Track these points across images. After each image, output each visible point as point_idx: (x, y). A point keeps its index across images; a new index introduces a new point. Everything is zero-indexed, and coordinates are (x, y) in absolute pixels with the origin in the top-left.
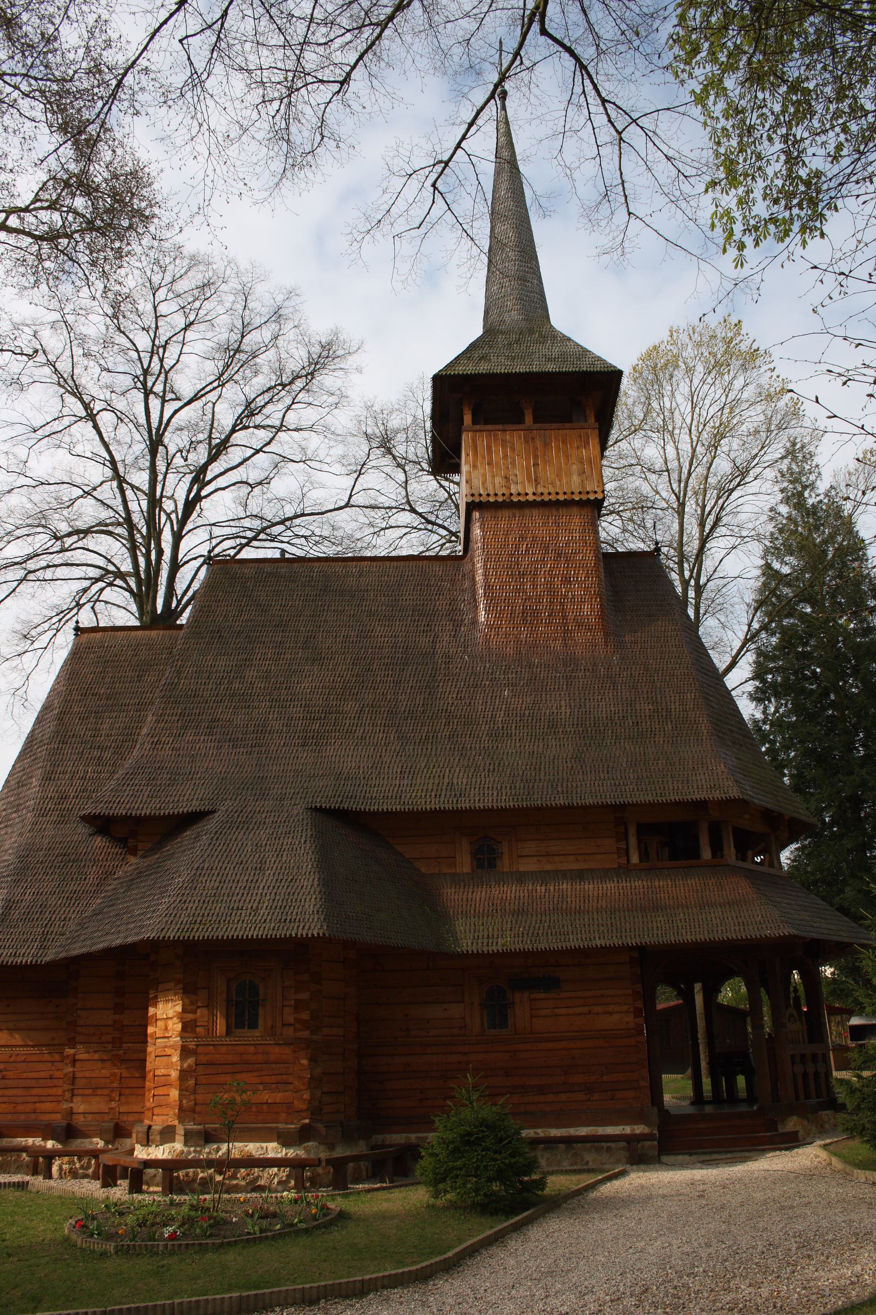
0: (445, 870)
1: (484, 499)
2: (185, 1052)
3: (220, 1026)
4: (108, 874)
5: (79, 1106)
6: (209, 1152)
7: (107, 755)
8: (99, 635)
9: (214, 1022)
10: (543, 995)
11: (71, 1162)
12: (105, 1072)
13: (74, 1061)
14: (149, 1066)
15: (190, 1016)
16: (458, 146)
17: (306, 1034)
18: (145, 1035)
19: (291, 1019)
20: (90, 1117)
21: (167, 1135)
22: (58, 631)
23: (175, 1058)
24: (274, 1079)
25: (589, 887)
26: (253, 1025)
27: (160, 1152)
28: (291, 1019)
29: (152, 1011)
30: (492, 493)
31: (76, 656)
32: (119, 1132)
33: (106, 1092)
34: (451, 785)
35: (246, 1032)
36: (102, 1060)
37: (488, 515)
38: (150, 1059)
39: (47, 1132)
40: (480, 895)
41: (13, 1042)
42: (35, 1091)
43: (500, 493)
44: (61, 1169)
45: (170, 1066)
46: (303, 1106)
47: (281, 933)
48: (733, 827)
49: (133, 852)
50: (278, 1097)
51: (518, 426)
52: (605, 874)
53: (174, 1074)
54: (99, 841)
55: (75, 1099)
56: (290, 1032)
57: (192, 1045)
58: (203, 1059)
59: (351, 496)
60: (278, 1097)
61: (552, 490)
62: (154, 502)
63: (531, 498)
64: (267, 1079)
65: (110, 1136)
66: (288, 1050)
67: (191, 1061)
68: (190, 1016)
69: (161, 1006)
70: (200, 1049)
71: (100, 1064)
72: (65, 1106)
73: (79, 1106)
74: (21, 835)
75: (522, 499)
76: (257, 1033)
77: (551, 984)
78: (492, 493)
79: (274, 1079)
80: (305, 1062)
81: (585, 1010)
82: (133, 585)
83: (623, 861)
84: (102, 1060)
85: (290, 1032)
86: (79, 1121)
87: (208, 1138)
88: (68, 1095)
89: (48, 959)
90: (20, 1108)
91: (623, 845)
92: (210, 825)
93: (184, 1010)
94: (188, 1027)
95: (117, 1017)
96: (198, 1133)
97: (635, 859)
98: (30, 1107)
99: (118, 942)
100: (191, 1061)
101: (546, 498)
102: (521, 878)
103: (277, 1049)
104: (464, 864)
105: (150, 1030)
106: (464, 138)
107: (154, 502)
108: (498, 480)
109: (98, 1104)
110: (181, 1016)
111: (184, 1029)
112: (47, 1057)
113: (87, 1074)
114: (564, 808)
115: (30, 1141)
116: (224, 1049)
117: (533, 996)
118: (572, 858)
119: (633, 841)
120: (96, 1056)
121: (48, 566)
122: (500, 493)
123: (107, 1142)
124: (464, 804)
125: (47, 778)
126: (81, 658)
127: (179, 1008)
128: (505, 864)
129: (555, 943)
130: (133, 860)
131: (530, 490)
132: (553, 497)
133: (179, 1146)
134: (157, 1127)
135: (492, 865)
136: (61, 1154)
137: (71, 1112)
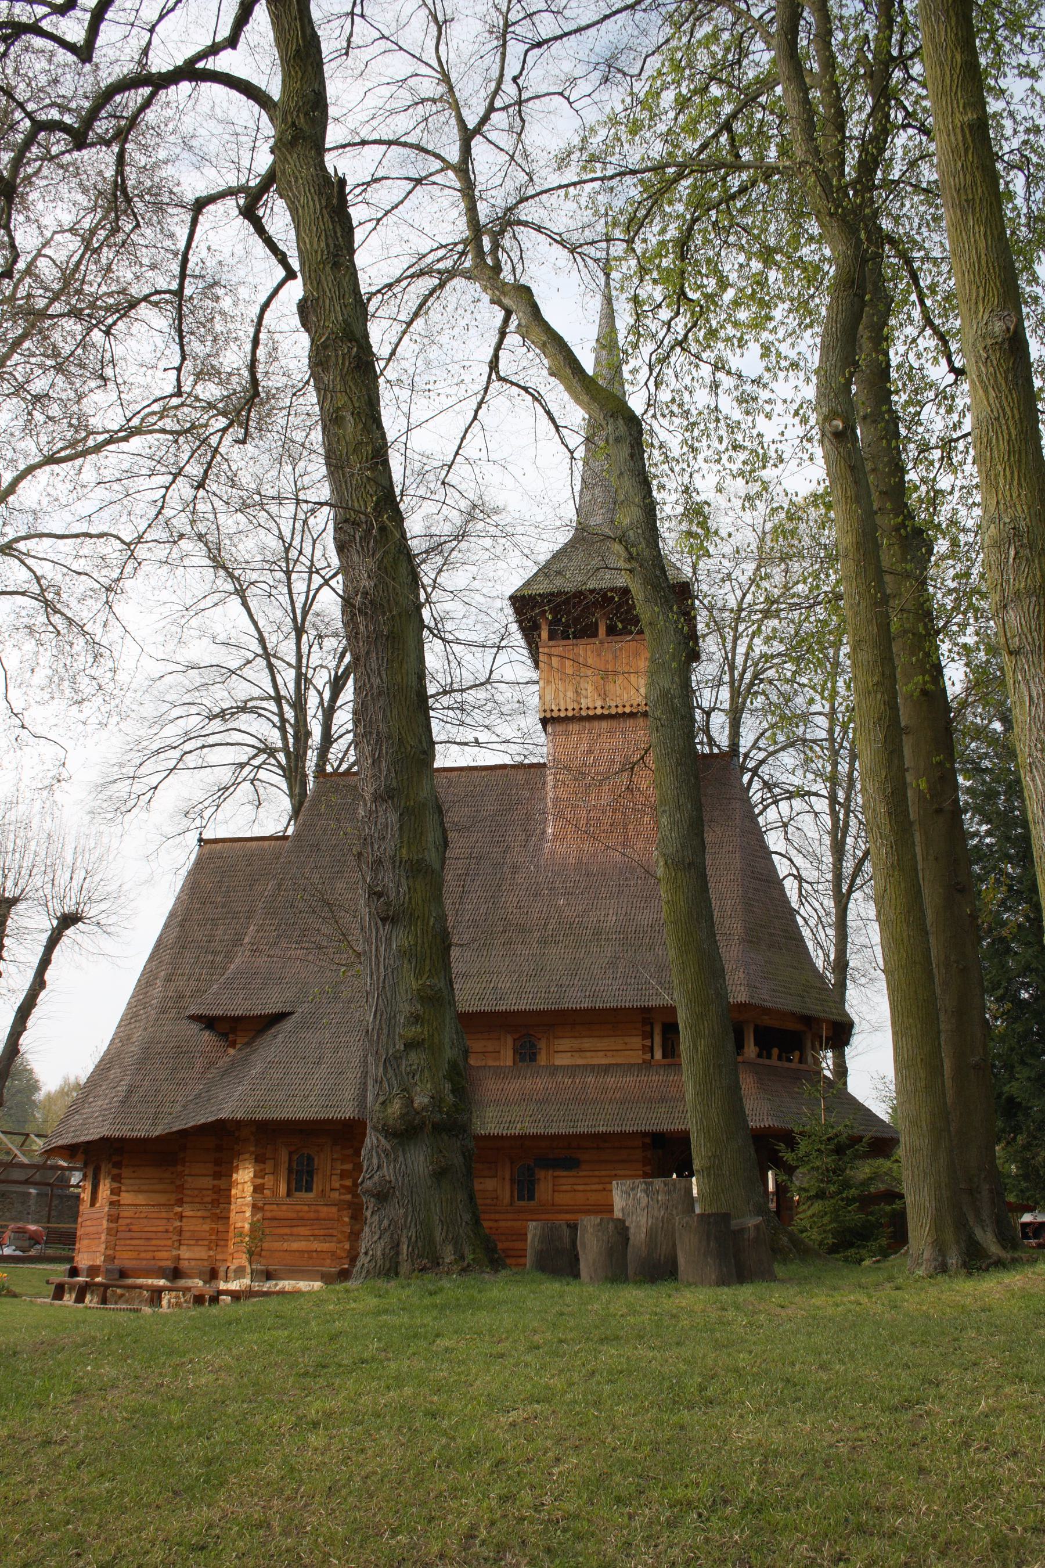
0: (491, 1063)
1: (555, 714)
2: (255, 1207)
3: (283, 1189)
4: (212, 1064)
5: (185, 1253)
6: (268, 1286)
7: (219, 959)
8: (219, 846)
9: (278, 1186)
10: (565, 1173)
11: (177, 1297)
12: (206, 1227)
13: (181, 1217)
14: (232, 1221)
15: (259, 1181)
16: (457, 453)
17: (349, 1197)
18: (229, 1196)
19: (337, 1185)
20: (193, 1263)
21: (240, 1273)
22: (218, 806)
23: (248, 1214)
24: (322, 1232)
25: (611, 1080)
26: (309, 1189)
27: (234, 1286)
28: (337, 1185)
29: (235, 1176)
30: (563, 708)
31: (200, 866)
32: (213, 1275)
33: (206, 1243)
34: (495, 988)
35: (303, 1195)
36: (203, 1218)
37: (559, 728)
38: (232, 1215)
39: (161, 1273)
40: (514, 1086)
41: (138, 1202)
42: (154, 1242)
43: (570, 708)
44: (169, 1302)
45: (244, 1220)
46: (344, 1255)
47: (322, 1116)
48: (756, 1027)
49: (233, 1045)
50: (325, 1246)
51: (593, 640)
52: (628, 1068)
53: (247, 1226)
54: (207, 1035)
55: (183, 1248)
56: (335, 1195)
57: (260, 1204)
58: (268, 1215)
59: (491, 672)
60: (325, 1246)
61: (619, 703)
62: (302, 680)
63: (599, 711)
64: (316, 1232)
65: (207, 1278)
66: (334, 1209)
67: (259, 1216)
68: (259, 1181)
69: (240, 1172)
70: (267, 1207)
71: (201, 1221)
72: (175, 1253)
73: (185, 1253)
74: (145, 1029)
75: (591, 713)
76: (311, 1195)
77: (570, 1164)
78: (563, 708)
79: (322, 1232)
80: (346, 1219)
81: (600, 1187)
82: (284, 762)
83: (648, 1056)
84: (203, 1218)
85: (335, 1195)
86: (184, 1265)
87: (269, 1276)
88: (176, 1244)
89: (157, 1133)
90: (143, 1255)
91: (648, 1043)
92: (288, 1025)
93: (255, 1176)
94: (258, 1189)
95: (216, 1182)
96: (262, 1271)
97: (658, 1055)
98: (149, 1255)
99: (203, 1121)
100: (259, 1216)
101: (613, 711)
102: (554, 1070)
103: (325, 1209)
104: (507, 1058)
105: (233, 1192)
106: (459, 447)
107: (302, 680)
108: (570, 694)
109: (201, 1252)
110: (252, 1181)
111: (255, 1191)
112: (164, 1215)
113: (192, 1228)
114: (586, 1011)
115: (150, 1281)
116: (284, 1207)
117: (556, 1173)
118: (602, 1054)
119: (658, 1039)
120: (199, 1214)
121: (204, 747)
122: (570, 708)
123: (205, 1282)
124: (502, 1007)
125: (169, 979)
126: (202, 868)
127: (252, 1175)
128: (542, 1060)
129: (564, 1129)
130: (232, 1051)
131: (599, 704)
132: (620, 710)
133: (246, 1281)
134: (233, 1267)
135: (533, 1058)
136: (170, 1290)
137: (178, 1258)
